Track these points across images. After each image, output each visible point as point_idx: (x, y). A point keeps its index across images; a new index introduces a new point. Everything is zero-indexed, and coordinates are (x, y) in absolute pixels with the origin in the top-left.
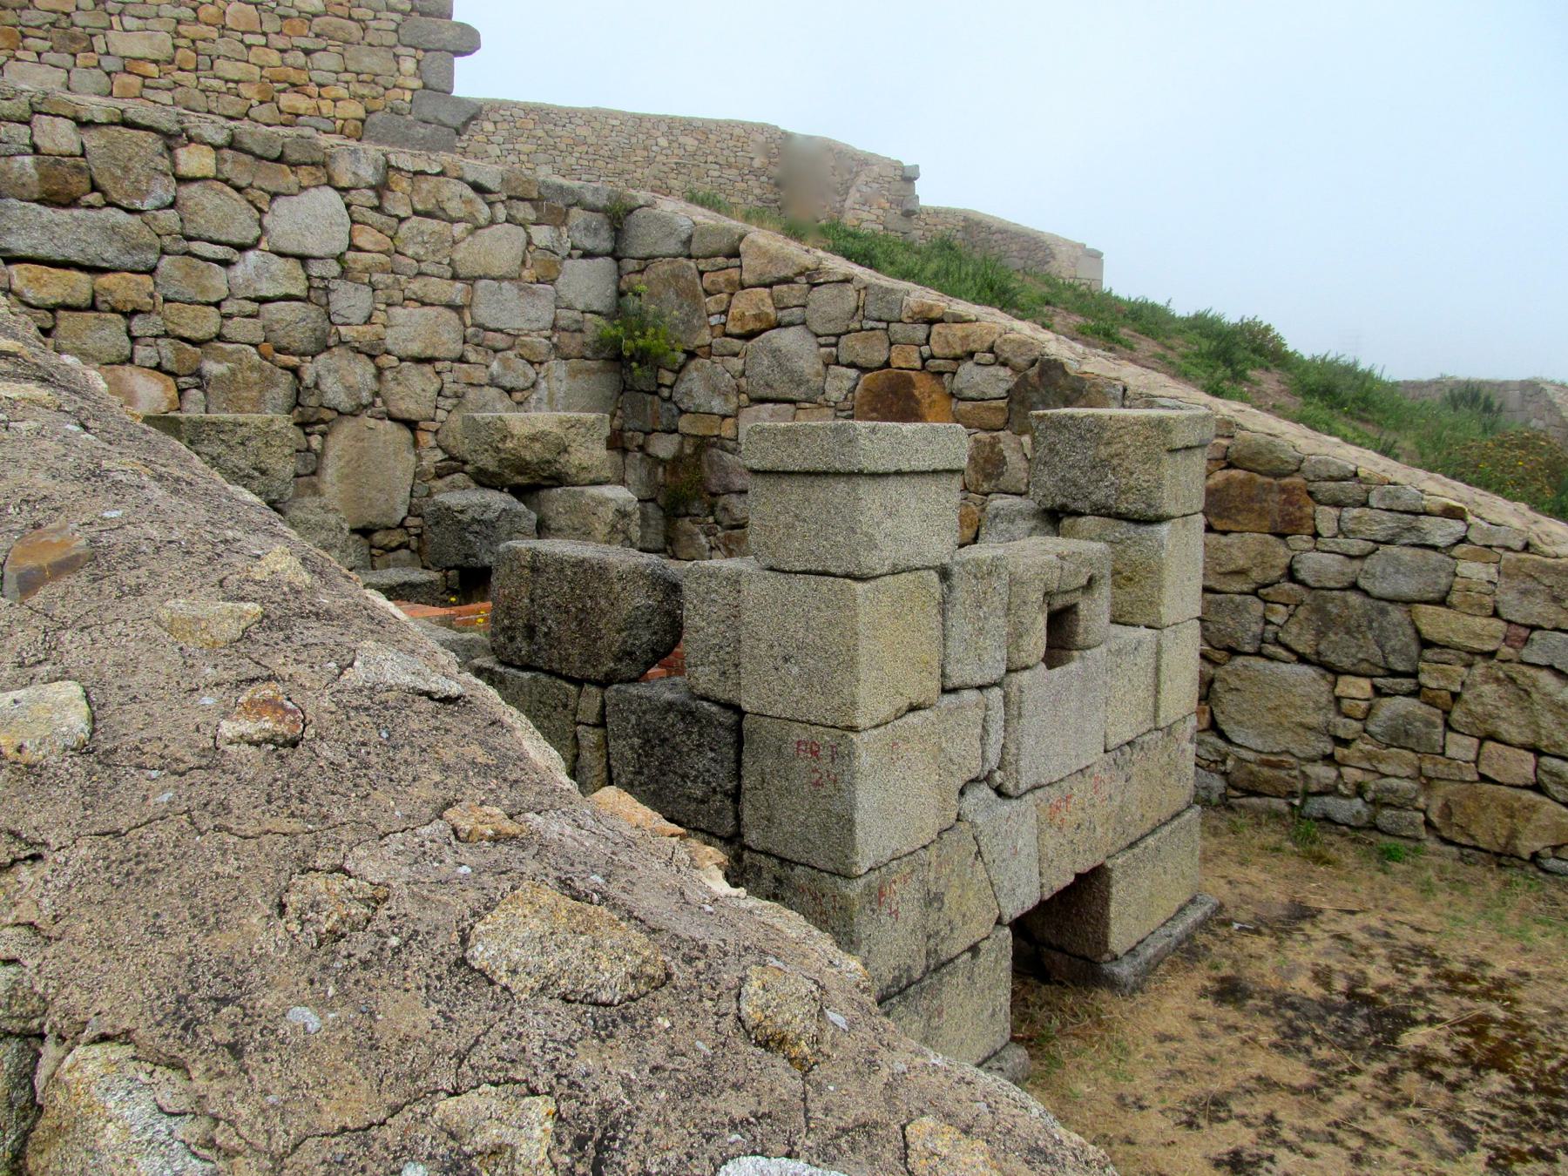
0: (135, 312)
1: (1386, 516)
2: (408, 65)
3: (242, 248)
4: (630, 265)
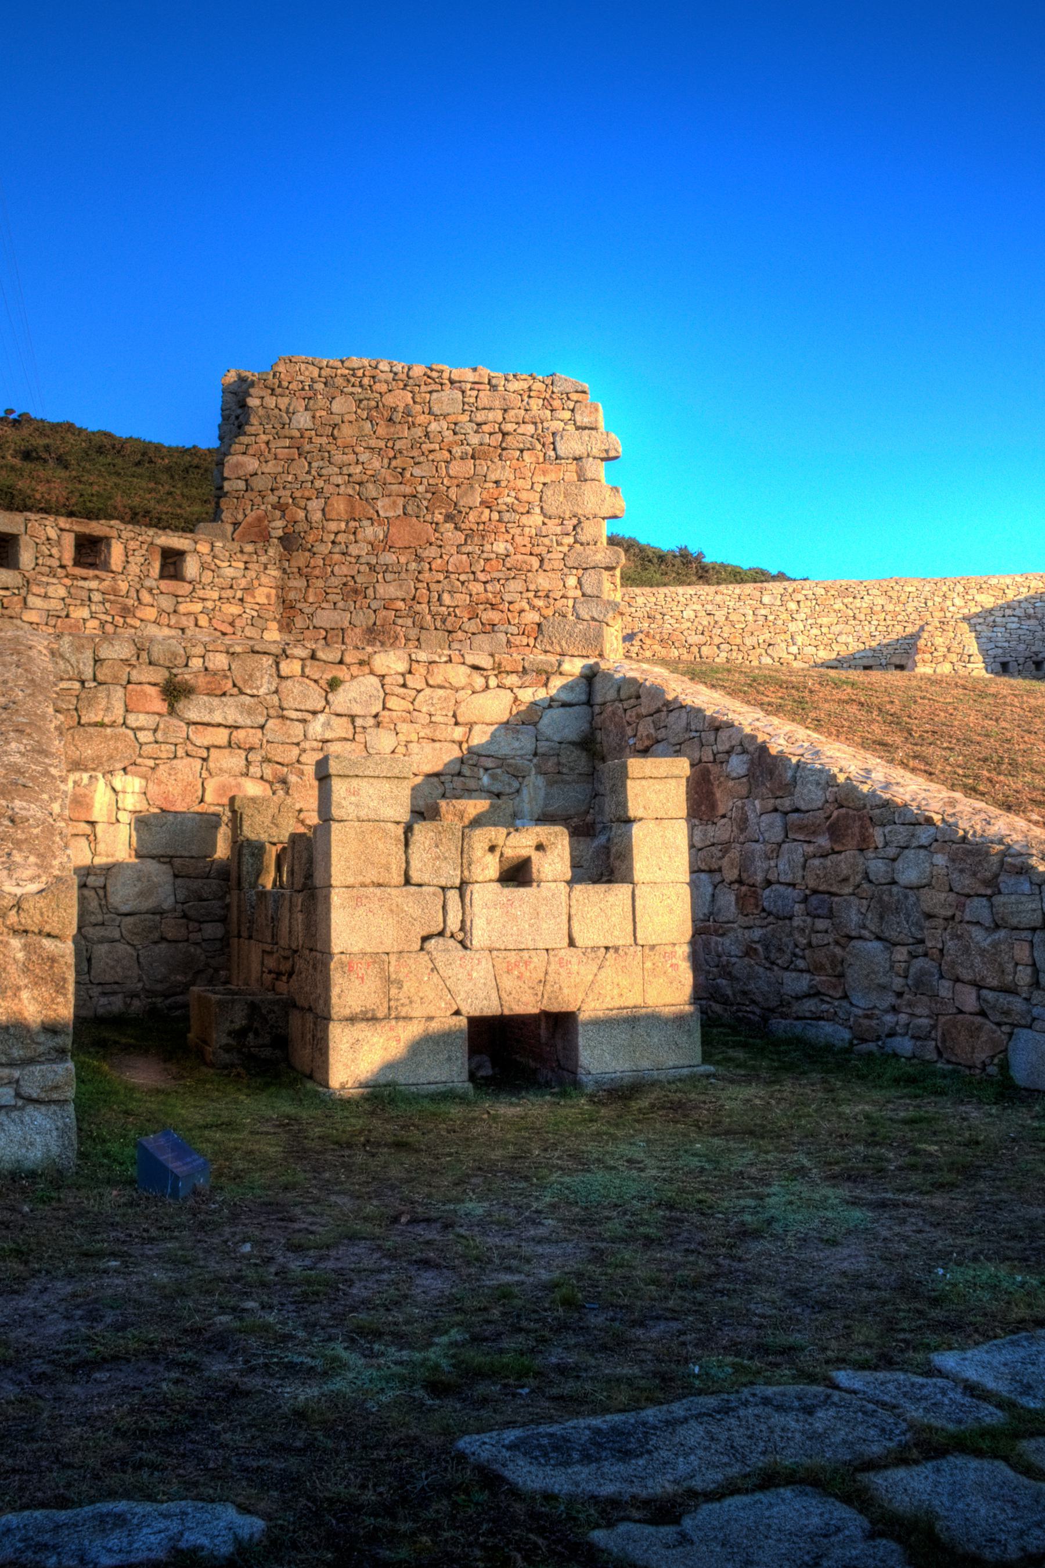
0: (251, 749)
1: (902, 829)
2: (572, 581)
3: (314, 713)
4: (597, 709)
